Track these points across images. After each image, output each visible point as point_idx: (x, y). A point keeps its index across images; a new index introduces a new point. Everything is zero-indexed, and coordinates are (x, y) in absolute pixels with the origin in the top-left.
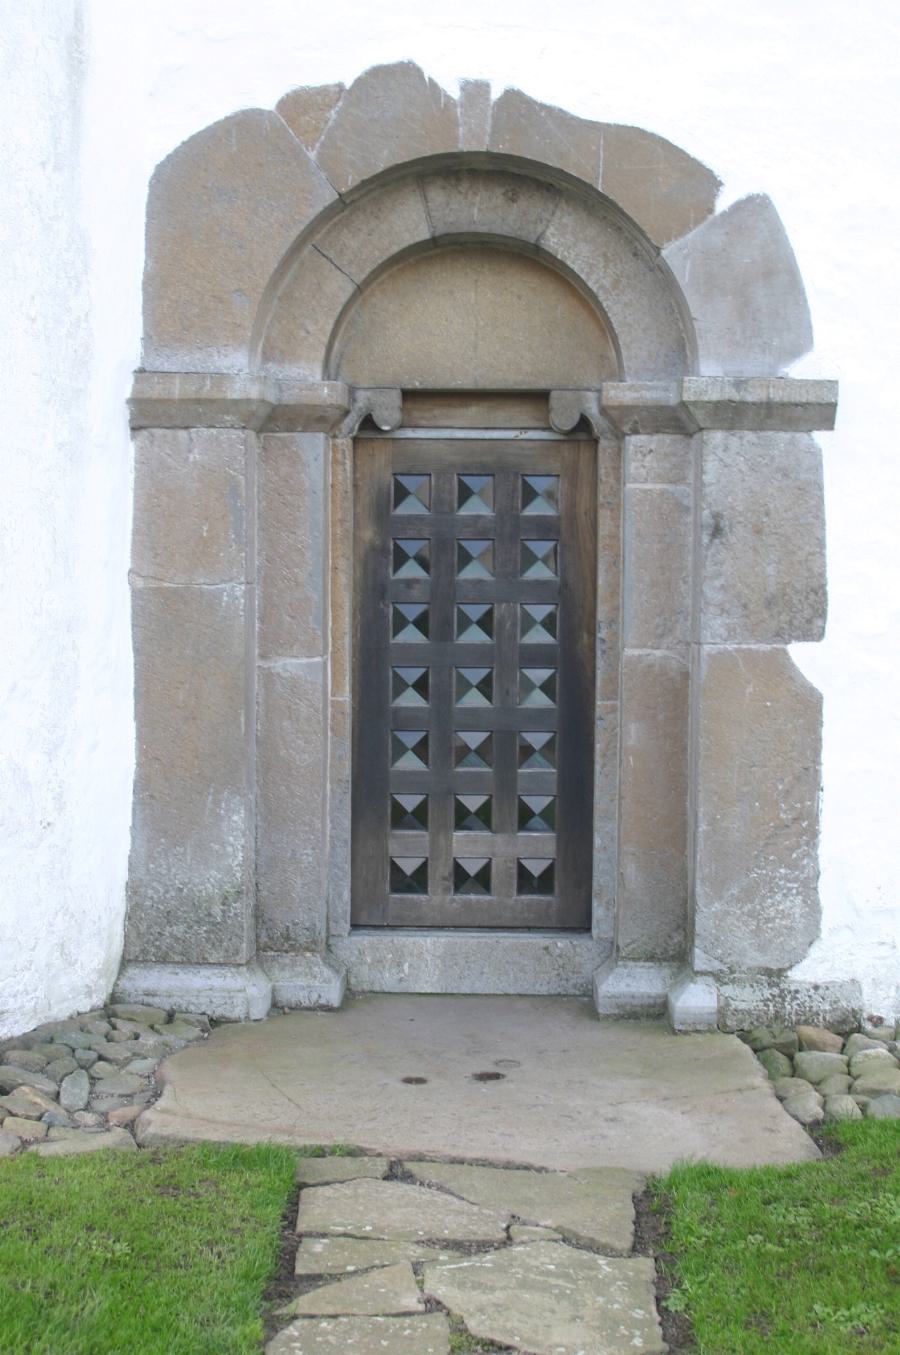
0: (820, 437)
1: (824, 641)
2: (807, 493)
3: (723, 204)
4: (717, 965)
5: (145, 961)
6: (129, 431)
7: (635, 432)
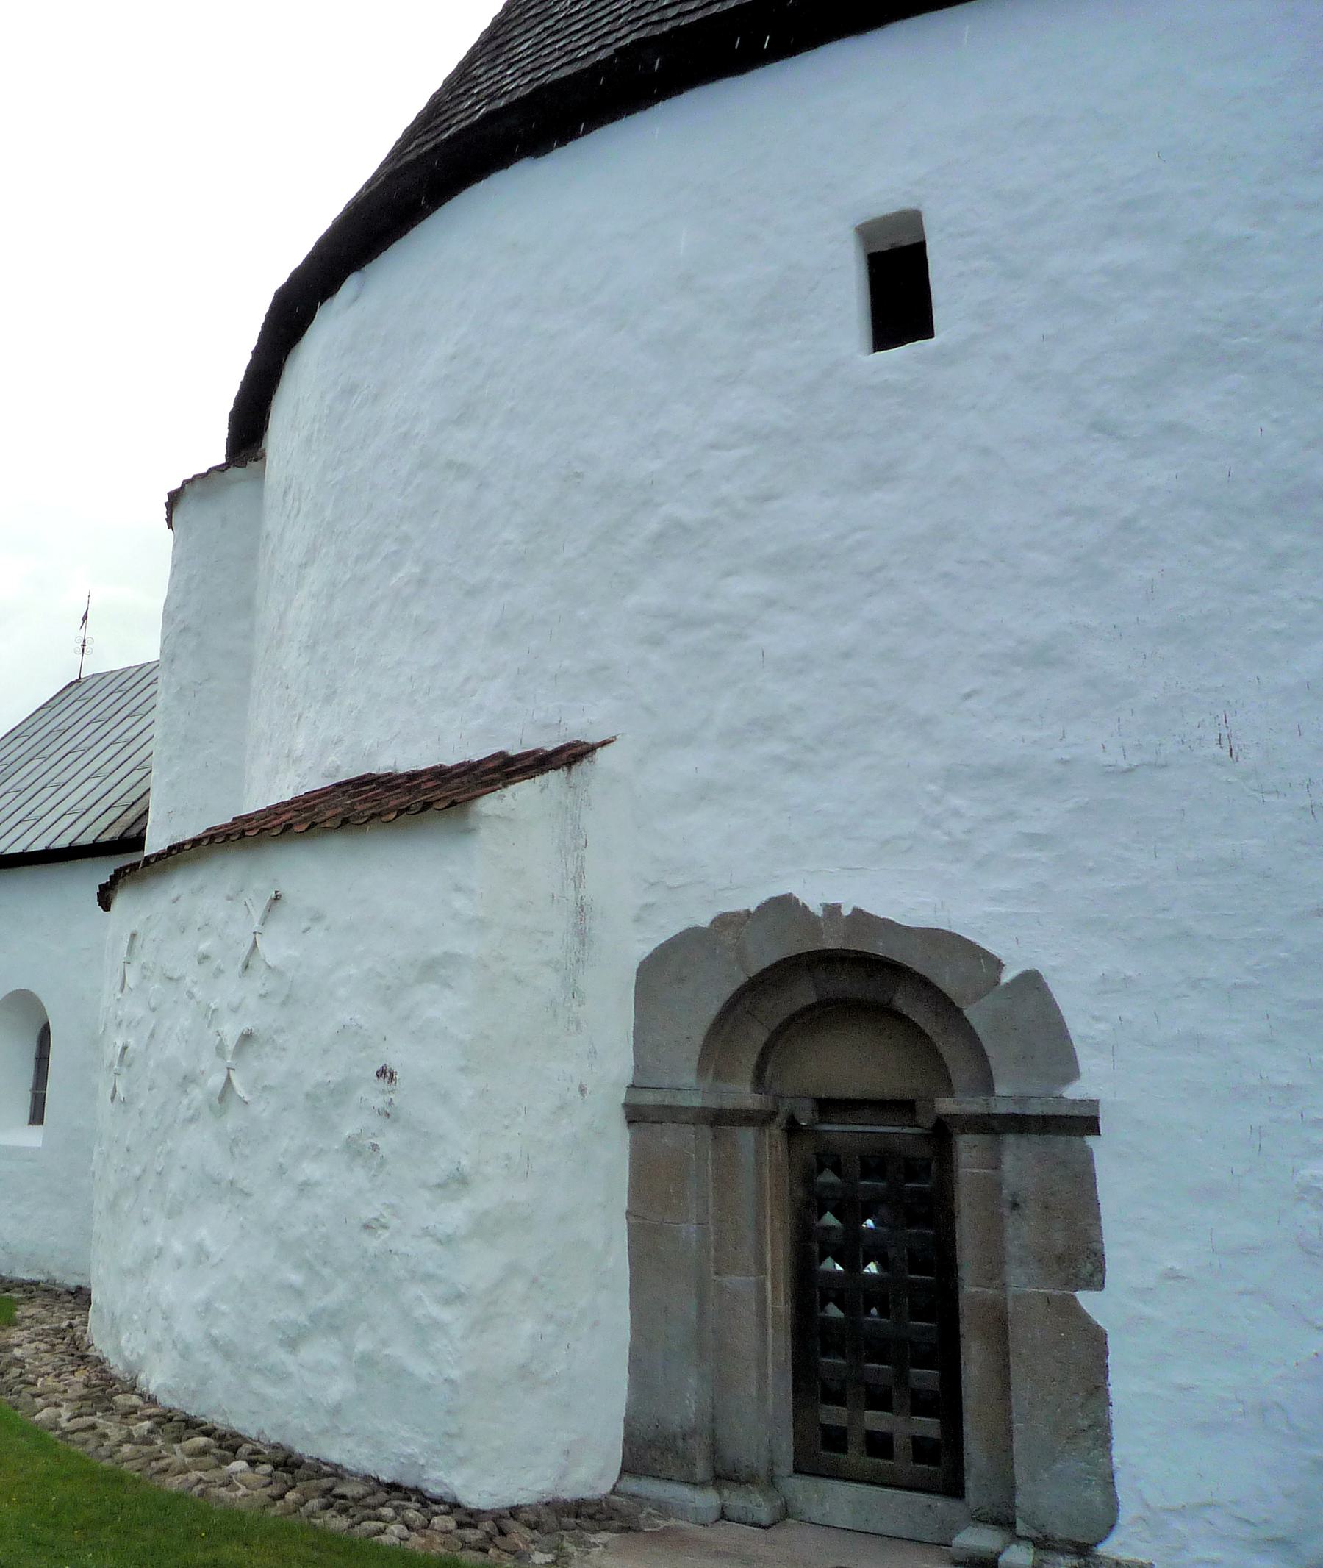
0: (1090, 1140)
1: (1105, 1291)
2: (1084, 1179)
3: (1006, 978)
4: (1034, 1534)
5: (635, 1473)
6: (626, 1124)
7: (963, 1132)
